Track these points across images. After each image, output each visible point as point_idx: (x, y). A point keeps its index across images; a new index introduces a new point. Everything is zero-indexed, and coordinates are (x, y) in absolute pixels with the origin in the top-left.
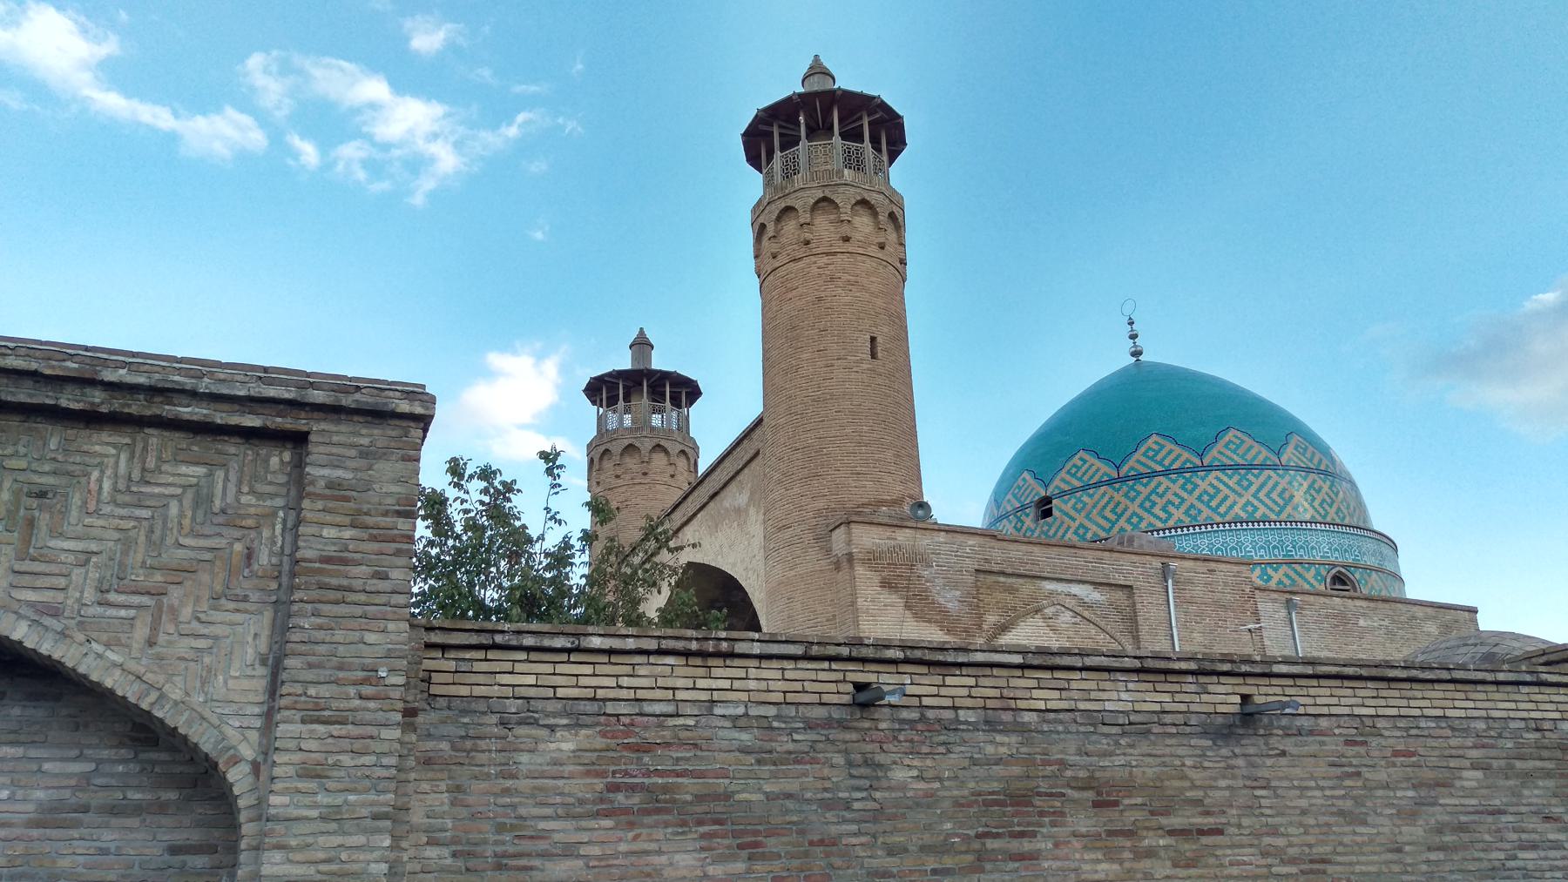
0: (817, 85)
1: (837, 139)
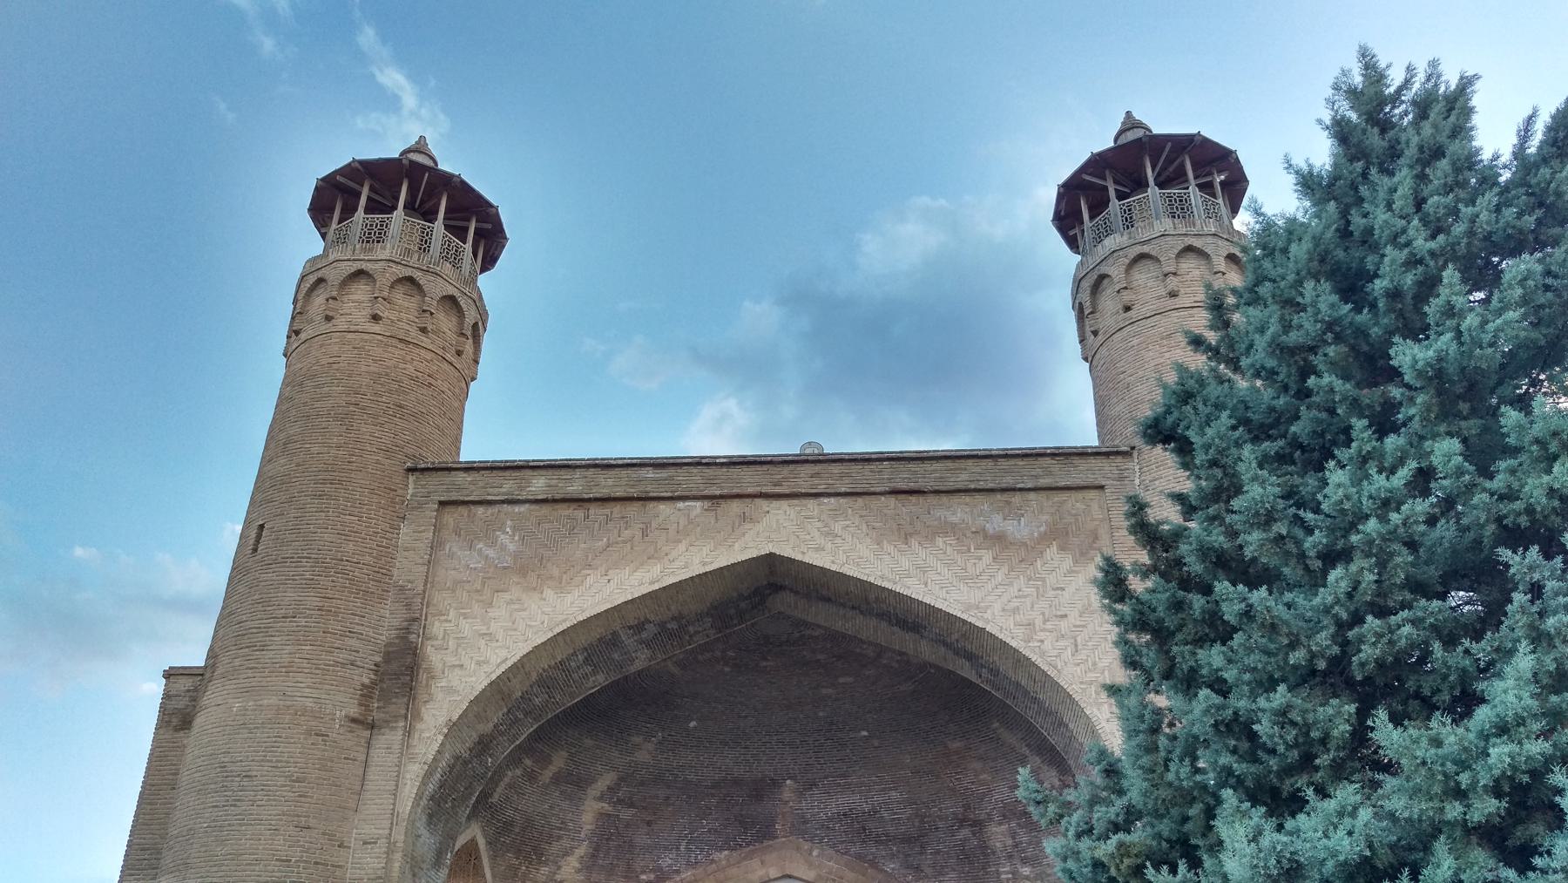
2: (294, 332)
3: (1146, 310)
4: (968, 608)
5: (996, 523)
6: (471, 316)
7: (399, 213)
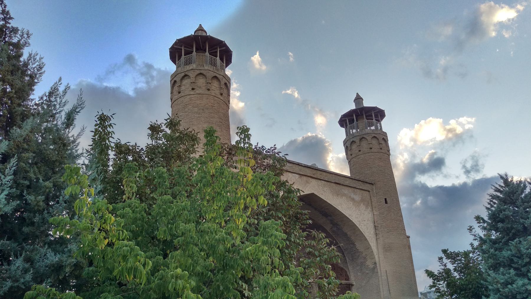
0: (200, 33)
1: (207, 53)
3: (375, 150)
4: (350, 215)
5: (353, 196)
6: (223, 81)
7: (194, 53)
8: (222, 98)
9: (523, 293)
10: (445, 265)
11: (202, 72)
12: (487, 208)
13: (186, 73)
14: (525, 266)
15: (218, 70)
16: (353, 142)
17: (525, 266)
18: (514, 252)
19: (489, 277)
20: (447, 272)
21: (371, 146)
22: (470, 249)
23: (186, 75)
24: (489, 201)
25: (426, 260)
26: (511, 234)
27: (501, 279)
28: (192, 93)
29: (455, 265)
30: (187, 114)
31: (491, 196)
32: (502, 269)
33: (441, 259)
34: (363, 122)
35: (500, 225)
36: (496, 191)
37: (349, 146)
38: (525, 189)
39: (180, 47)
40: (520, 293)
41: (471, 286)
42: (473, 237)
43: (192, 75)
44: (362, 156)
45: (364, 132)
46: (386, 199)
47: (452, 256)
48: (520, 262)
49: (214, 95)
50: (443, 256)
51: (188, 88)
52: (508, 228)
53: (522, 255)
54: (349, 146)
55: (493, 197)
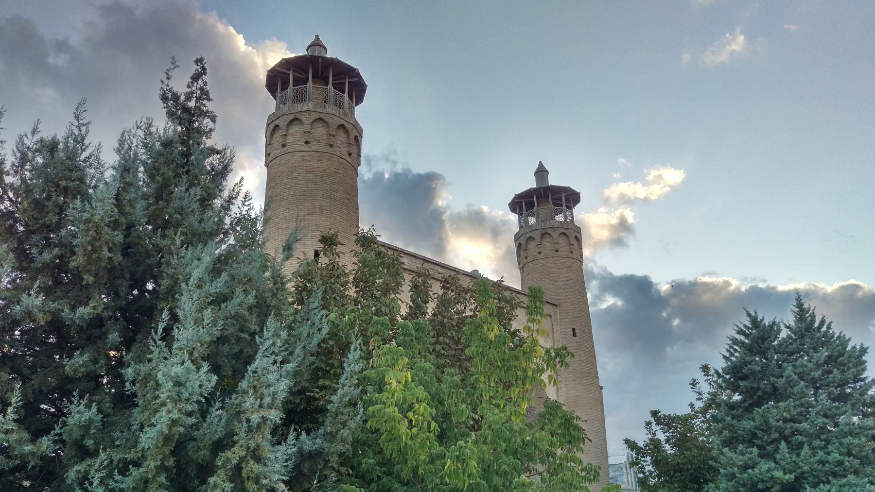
2: (268, 155)
3: (563, 254)
8: (350, 160)
9: (767, 482)
10: (654, 434)
11: (321, 116)
12: (725, 357)
13: (297, 116)
14: (772, 443)
15: (346, 115)
16: (530, 238)
17: (772, 443)
18: (758, 423)
19: (722, 457)
20: (655, 444)
21: (558, 247)
22: (688, 411)
23: (296, 119)
24: (727, 347)
25: (623, 426)
26: (755, 397)
27: (740, 460)
28: (305, 148)
29: (667, 434)
30: (295, 181)
31: (732, 340)
32: (741, 447)
33: (649, 424)
34: (545, 204)
35: (742, 383)
36: (738, 333)
37: (523, 243)
38: (779, 334)
39: (287, 72)
40: (763, 481)
41: (690, 467)
42: (696, 396)
43: (306, 119)
44: (543, 261)
45: (548, 225)
46: (574, 329)
47: (667, 422)
48: (766, 438)
49: (339, 154)
50: (652, 420)
51: (298, 141)
52: (752, 388)
53: (770, 428)
54: (523, 243)
55: (735, 341)
